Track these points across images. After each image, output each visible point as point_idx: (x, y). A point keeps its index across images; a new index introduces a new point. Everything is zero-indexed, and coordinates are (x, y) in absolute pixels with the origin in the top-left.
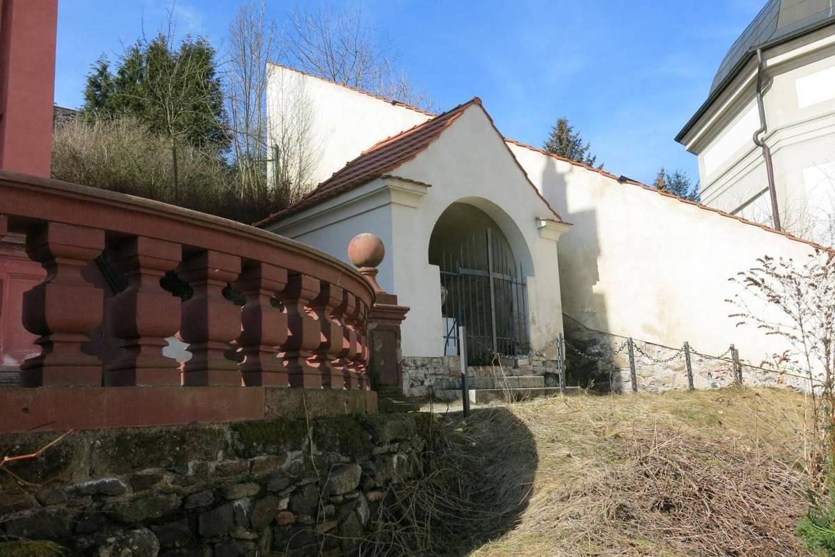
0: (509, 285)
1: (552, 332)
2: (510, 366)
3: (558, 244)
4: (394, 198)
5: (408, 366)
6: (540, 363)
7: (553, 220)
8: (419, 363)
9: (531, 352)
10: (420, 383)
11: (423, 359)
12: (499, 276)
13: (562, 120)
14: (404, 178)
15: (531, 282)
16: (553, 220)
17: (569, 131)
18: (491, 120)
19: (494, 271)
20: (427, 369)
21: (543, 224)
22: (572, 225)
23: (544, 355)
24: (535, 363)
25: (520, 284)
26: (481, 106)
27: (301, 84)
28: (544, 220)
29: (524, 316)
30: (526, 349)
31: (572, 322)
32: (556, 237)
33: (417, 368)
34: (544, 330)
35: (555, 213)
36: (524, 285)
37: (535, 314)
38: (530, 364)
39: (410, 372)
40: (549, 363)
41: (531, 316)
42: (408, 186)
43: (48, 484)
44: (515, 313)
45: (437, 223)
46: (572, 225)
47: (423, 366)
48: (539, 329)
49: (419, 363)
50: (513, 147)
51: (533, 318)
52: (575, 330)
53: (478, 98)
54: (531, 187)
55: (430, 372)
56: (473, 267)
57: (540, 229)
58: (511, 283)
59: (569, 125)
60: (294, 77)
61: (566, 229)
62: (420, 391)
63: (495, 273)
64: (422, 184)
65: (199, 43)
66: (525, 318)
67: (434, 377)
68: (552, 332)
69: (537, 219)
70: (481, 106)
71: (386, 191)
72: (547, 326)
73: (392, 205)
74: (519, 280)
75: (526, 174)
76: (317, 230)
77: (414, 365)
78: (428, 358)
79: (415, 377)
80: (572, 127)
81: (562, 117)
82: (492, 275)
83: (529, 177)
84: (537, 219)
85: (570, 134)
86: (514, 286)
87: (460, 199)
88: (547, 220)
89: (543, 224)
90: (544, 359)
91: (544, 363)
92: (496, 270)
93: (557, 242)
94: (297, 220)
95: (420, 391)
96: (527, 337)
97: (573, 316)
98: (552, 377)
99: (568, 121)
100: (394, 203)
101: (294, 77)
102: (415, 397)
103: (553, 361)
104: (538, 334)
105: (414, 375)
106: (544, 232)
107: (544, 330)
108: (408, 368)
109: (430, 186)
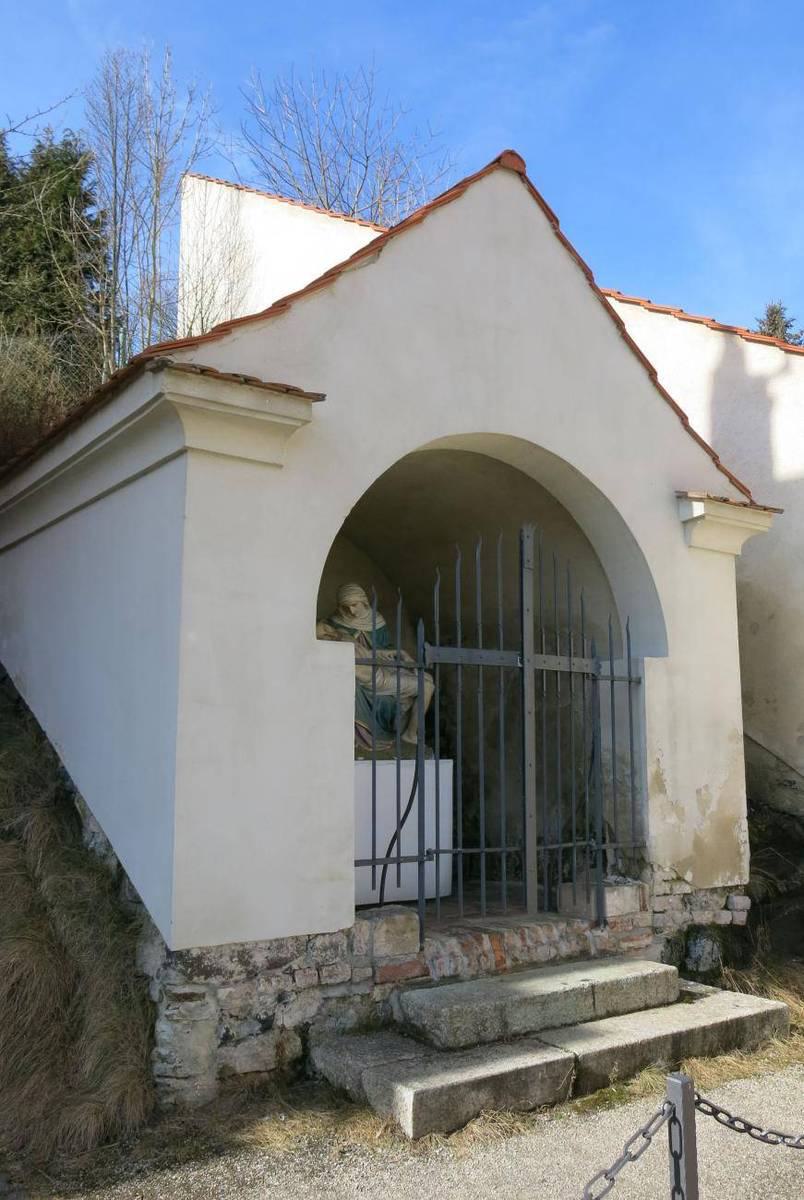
0: (588, 683)
1: (713, 807)
2: (583, 919)
3: (741, 565)
4: (194, 434)
5: (218, 972)
6: (675, 901)
7: (725, 501)
8: (259, 959)
9: (647, 872)
10: (258, 1027)
11: (280, 944)
12: (556, 663)
13: (775, 307)
14: (265, 380)
15: (654, 674)
16: (725, 501)
17: (786, 326)
18: (552, 218)
19: (538, 649)
20: (292, 973)
21: (698, 509)
22: (781, 511)
23: (689, 876)
24: (658, 904)
25: (621, 679)
26: (522, 175)
27: (235, 208)
28: (700, 500)
29: (633, 764)
30: (635, 864)
31: (772, 763)
32: (735, 543)
33: (252, 975)
34: (690, 805)
35: (733, 480)
36: (635, 683)
37: (665, 764)
38: (644, 908)
39: (223, 993)
40: (702, 897)
41: (651, 769)
42: (241, 398)
43: (55, 837)
44: (606, 756)
45: (353, 511)
46: (781, 511)
47: (274, 964)
48: (675, 807)
49: (259, 959)
50: (620, 309)
51: (658, 777)
52: (780, 784)
53: (512, 153)
54: (667, 408)
55: (301, 982)
56: (469, 641)
57: (688, 523)
58: (595, 679)
59: (788, 315)
60: (225, 196)
61: (762, 523)
62: (255, 1056)
63: (543, 657)
64: (288, 391)
65: (67, 144)
66: (633, 774)
67: (318, 994)
68: (713, 807)
69: (682, 497)
70: (522, 175)
71: (161, 414)
72: (698, 792)
73: (191, 459)
74: (621, 668)
75: (652, 374)
76: (43, 529)
77: (240, 968)
78: (297, 938)
79: (242, 1009)
80: (793, 320)
81: (776, 303)
82: (534, 662)
83: (661, 380)
84: (682, 497)
85: (788, 331)
86: (604, 686)
87: (432, 443)
88: (708, 499)
89: (698, 509)
90: (687, 889)
91: (686, 900)
92: (548, 642)
93: (736, 556)
94: (15, 493)
95: (255, 1056)
96: (638, 831)
97: (777, 748)
98: (709, 937)
99: (785, 309)
100: (193, 449)
101: (225, 196)
102: (234, 1075)
103: (714, 890)
104: (672, 819)
105: (238, 1003)
106: (699, 535)
107: (690, 805)
108: (214, 981)
109: (320, 397)
